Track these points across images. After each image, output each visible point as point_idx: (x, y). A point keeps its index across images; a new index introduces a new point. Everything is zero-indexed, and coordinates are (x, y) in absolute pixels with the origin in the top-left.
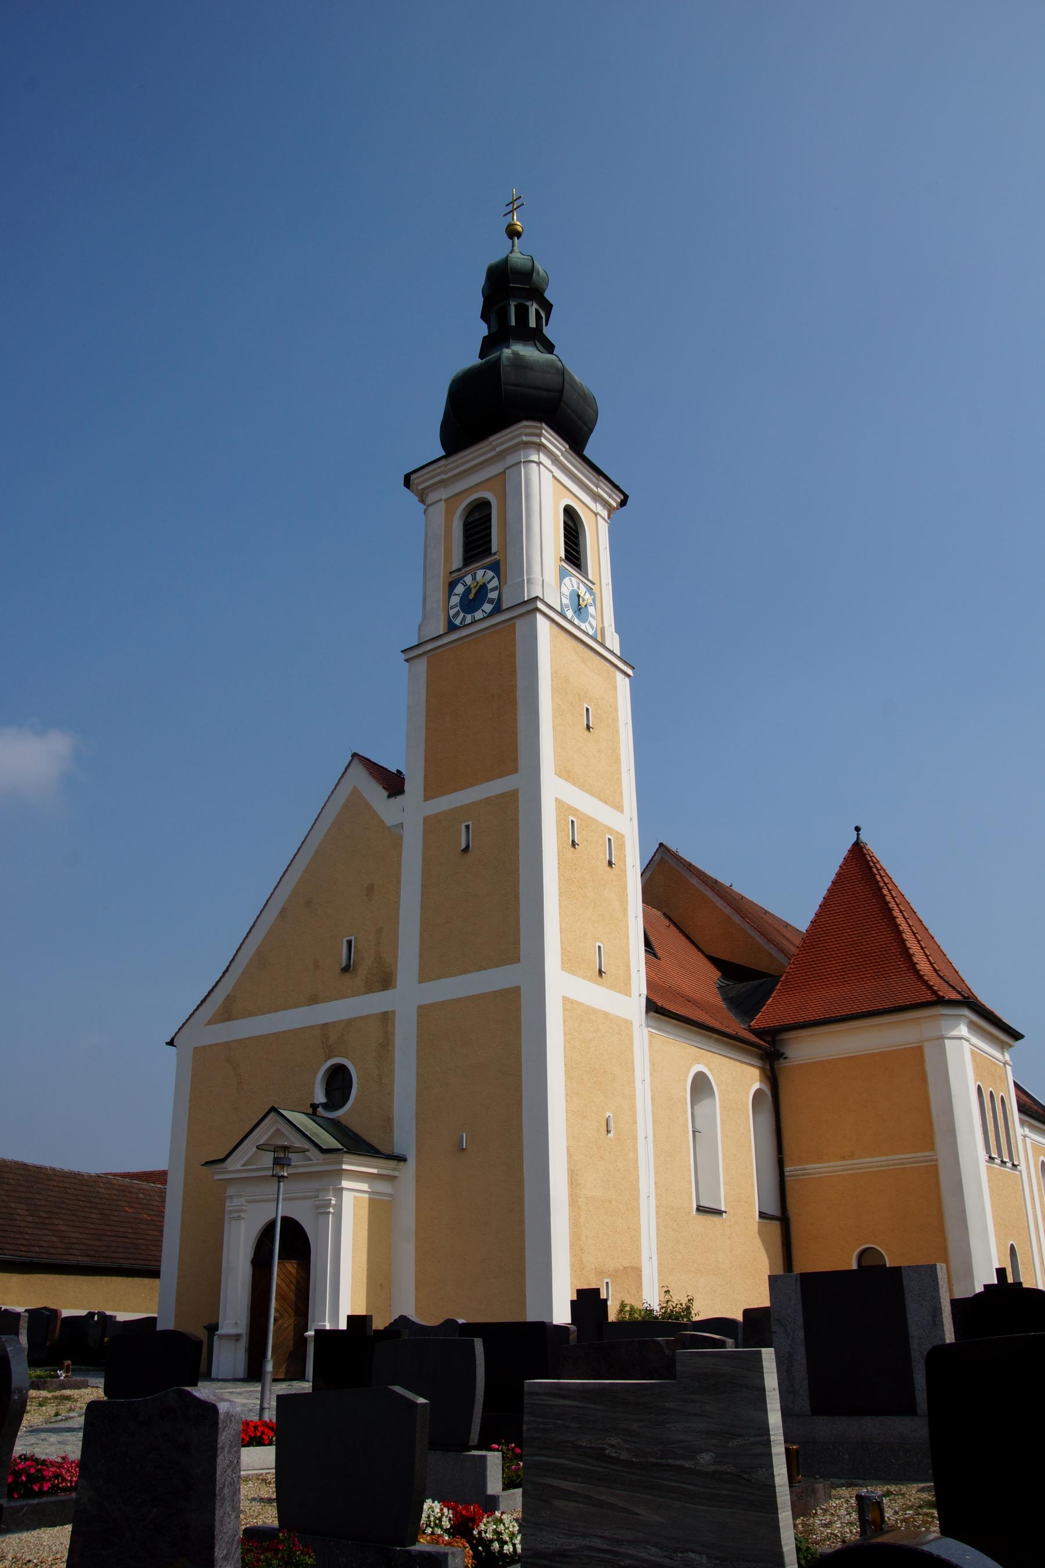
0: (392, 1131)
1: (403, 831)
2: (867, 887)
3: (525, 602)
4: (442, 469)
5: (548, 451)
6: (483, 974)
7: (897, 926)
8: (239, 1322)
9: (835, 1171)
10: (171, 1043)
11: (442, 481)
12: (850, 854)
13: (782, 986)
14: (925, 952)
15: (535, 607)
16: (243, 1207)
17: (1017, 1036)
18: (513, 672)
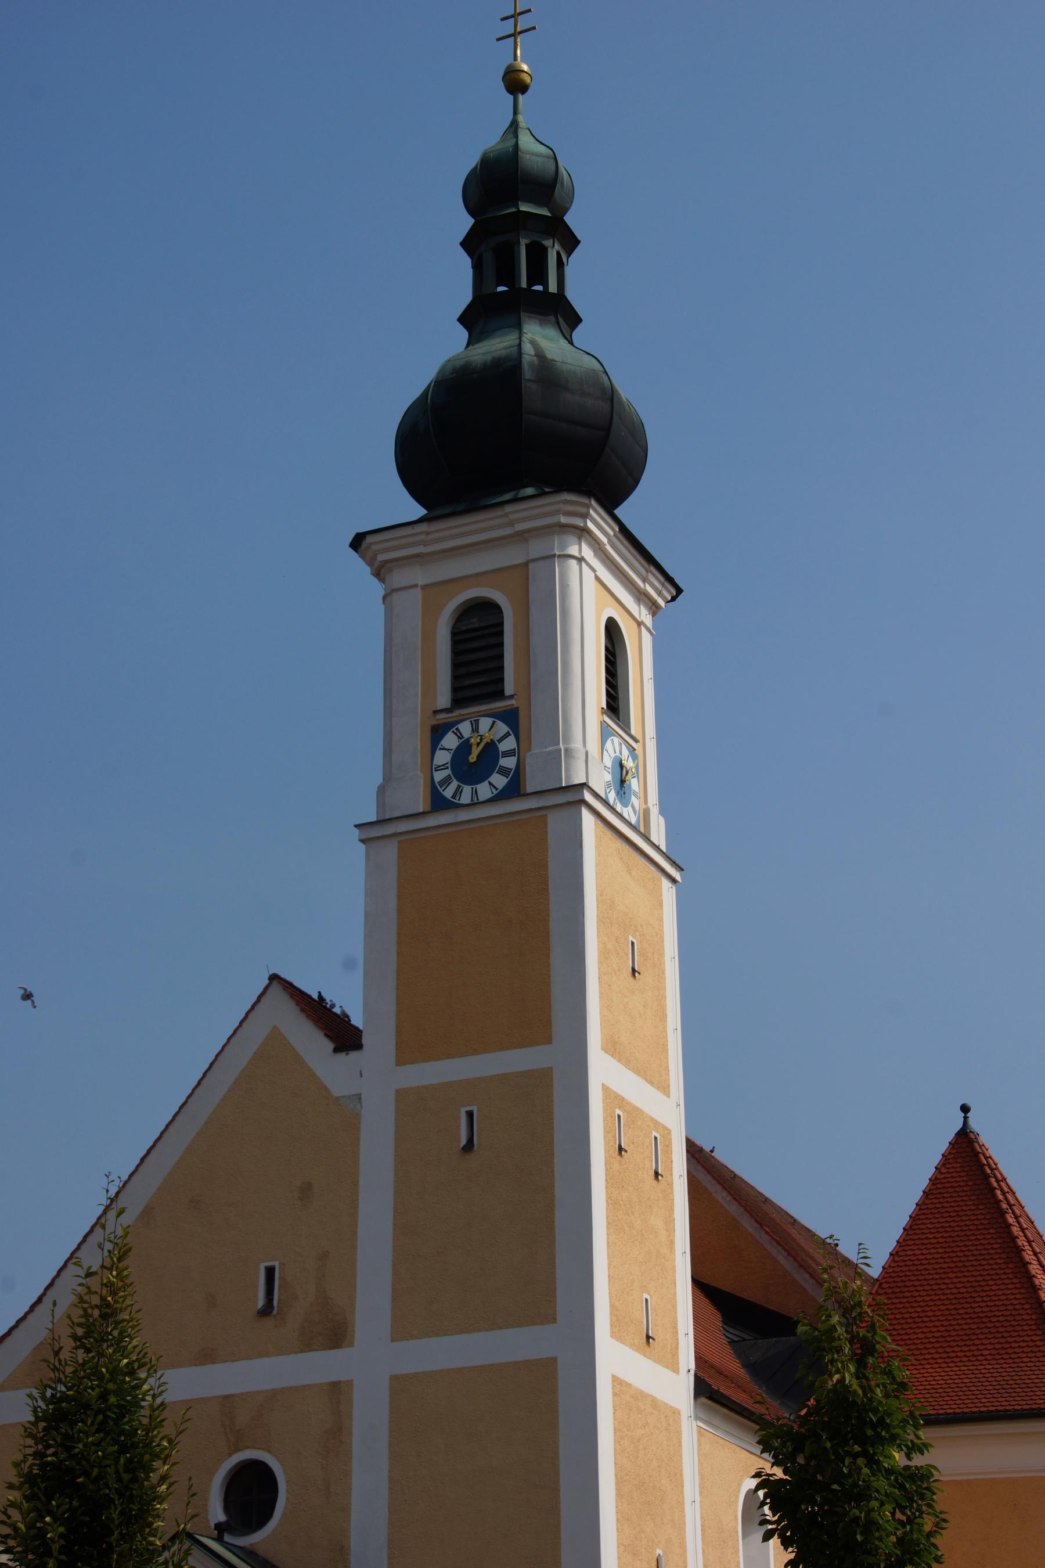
1: (361, 1106)
2: (982, 1207)
4: (423, 537)
5: (592, 538)
11: (418, 555)
17: (683, 870)
18: (544, 889)
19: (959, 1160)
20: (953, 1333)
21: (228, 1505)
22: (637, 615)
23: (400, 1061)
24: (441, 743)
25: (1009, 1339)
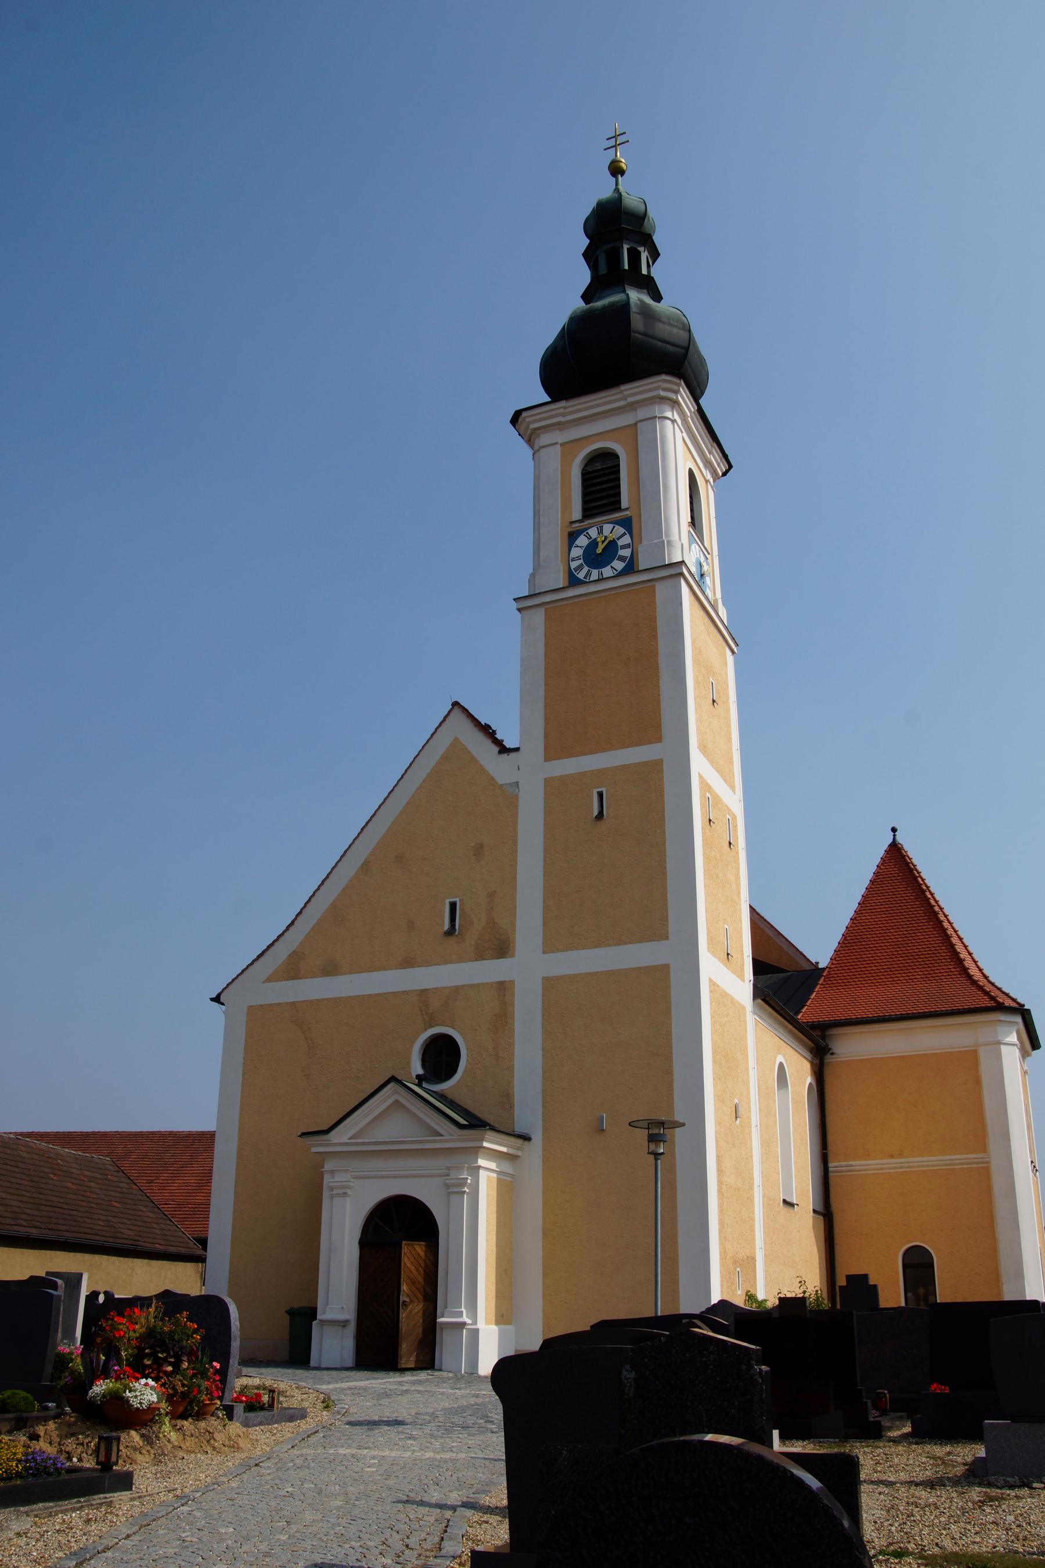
0: (512, 1107)
1: (519, 791)
3: (671, 565)
4: (562, 411)
5: (681, 410)
8: (345, 1307)
9: (882, 1169)
10: (217, 999)
11: (559, 424)
12: (887, 854)
13: (824, 981)
16: (351, 1184)
18: (654, 636)
19: (892, 861)
21: (424, 1065)
24: (576, 543)
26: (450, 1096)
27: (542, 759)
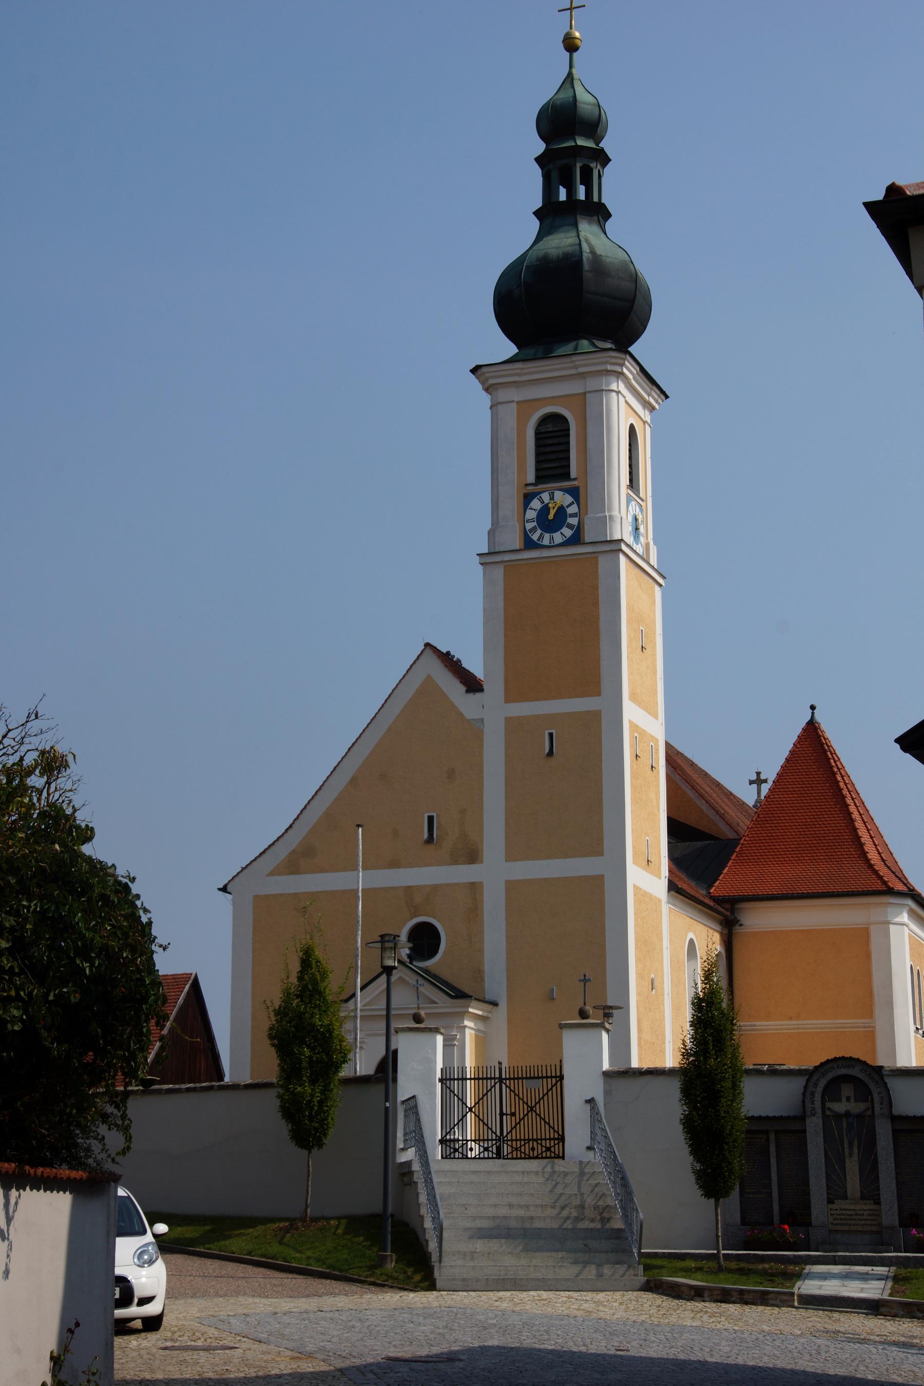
3: (611, 541)
4: (519, 371)
6: (569, 861)
7: (850, 814)
10: (224, 889)
13: (737, 856)
14: (873, 841)
15: (619, 548)
16: (365, 1040)
18: (596, 604)
20: (802, 846)
22: (643, 417)
23: (508, 700)
25: (836, 850)
26: (433, 970)
27: (503, 699)
